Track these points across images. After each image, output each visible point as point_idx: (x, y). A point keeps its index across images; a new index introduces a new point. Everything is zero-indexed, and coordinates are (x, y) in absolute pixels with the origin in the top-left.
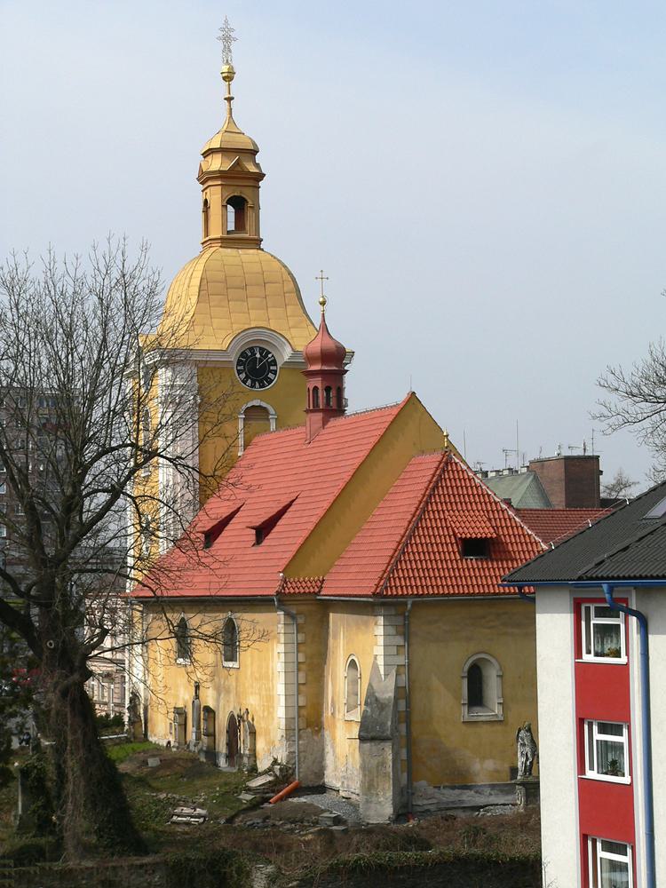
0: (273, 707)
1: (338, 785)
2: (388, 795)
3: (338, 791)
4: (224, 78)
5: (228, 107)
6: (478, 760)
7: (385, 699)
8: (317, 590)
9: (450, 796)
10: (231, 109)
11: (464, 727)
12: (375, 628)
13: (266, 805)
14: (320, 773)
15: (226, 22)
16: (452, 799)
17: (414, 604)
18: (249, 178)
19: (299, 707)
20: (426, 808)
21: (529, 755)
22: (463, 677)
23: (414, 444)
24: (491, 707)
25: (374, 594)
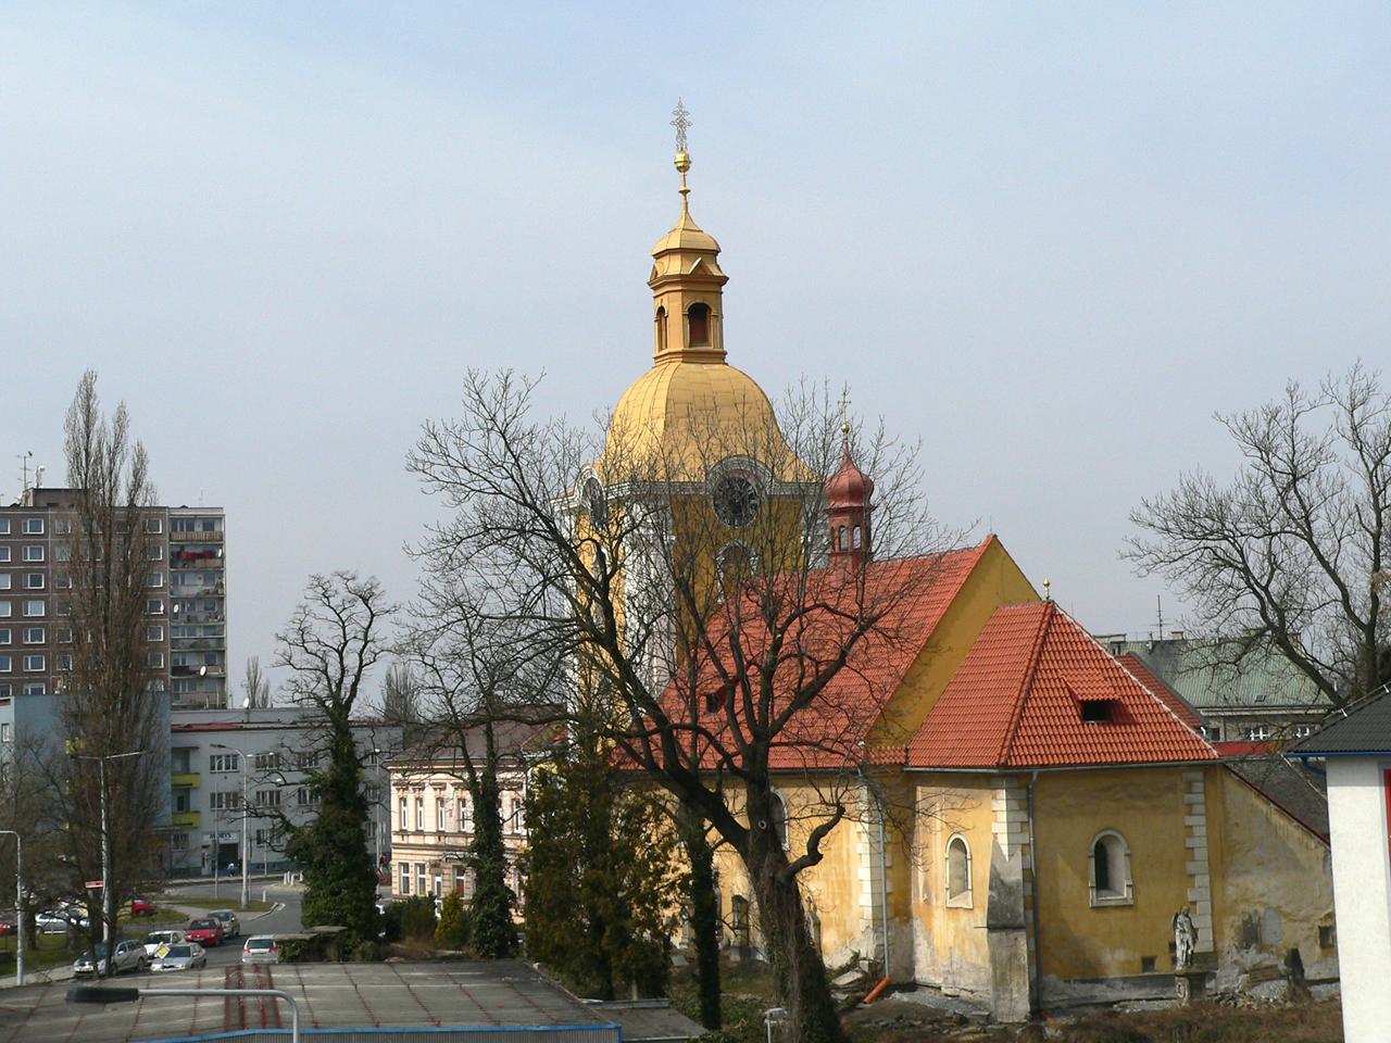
0: (850, 895)
1: (938, 981)
2: (1023, 990)
3: (940, 988)
4: (679, 168)
5: (683, 202)
6: (1108, 950)
7: (1013, 882)
8: (904, 761)
9: (1081, 991)
10: (687, 204)
11: (1093, 914)
12: (994, 803)
13: (861, 1005)
14: (910, 969)
15: (680, 105)
16: (1082, 995)
17: (1039, 775)
18: (713, 283)
19: (888, 894)
20: (1056, 1004)
21: (1190, 942)
22: (1090, 857)
23: (997, 593)
24: (1117, 889)
25: (998, 764)
